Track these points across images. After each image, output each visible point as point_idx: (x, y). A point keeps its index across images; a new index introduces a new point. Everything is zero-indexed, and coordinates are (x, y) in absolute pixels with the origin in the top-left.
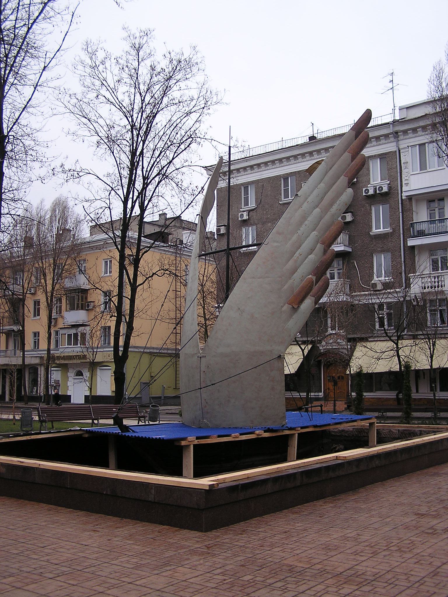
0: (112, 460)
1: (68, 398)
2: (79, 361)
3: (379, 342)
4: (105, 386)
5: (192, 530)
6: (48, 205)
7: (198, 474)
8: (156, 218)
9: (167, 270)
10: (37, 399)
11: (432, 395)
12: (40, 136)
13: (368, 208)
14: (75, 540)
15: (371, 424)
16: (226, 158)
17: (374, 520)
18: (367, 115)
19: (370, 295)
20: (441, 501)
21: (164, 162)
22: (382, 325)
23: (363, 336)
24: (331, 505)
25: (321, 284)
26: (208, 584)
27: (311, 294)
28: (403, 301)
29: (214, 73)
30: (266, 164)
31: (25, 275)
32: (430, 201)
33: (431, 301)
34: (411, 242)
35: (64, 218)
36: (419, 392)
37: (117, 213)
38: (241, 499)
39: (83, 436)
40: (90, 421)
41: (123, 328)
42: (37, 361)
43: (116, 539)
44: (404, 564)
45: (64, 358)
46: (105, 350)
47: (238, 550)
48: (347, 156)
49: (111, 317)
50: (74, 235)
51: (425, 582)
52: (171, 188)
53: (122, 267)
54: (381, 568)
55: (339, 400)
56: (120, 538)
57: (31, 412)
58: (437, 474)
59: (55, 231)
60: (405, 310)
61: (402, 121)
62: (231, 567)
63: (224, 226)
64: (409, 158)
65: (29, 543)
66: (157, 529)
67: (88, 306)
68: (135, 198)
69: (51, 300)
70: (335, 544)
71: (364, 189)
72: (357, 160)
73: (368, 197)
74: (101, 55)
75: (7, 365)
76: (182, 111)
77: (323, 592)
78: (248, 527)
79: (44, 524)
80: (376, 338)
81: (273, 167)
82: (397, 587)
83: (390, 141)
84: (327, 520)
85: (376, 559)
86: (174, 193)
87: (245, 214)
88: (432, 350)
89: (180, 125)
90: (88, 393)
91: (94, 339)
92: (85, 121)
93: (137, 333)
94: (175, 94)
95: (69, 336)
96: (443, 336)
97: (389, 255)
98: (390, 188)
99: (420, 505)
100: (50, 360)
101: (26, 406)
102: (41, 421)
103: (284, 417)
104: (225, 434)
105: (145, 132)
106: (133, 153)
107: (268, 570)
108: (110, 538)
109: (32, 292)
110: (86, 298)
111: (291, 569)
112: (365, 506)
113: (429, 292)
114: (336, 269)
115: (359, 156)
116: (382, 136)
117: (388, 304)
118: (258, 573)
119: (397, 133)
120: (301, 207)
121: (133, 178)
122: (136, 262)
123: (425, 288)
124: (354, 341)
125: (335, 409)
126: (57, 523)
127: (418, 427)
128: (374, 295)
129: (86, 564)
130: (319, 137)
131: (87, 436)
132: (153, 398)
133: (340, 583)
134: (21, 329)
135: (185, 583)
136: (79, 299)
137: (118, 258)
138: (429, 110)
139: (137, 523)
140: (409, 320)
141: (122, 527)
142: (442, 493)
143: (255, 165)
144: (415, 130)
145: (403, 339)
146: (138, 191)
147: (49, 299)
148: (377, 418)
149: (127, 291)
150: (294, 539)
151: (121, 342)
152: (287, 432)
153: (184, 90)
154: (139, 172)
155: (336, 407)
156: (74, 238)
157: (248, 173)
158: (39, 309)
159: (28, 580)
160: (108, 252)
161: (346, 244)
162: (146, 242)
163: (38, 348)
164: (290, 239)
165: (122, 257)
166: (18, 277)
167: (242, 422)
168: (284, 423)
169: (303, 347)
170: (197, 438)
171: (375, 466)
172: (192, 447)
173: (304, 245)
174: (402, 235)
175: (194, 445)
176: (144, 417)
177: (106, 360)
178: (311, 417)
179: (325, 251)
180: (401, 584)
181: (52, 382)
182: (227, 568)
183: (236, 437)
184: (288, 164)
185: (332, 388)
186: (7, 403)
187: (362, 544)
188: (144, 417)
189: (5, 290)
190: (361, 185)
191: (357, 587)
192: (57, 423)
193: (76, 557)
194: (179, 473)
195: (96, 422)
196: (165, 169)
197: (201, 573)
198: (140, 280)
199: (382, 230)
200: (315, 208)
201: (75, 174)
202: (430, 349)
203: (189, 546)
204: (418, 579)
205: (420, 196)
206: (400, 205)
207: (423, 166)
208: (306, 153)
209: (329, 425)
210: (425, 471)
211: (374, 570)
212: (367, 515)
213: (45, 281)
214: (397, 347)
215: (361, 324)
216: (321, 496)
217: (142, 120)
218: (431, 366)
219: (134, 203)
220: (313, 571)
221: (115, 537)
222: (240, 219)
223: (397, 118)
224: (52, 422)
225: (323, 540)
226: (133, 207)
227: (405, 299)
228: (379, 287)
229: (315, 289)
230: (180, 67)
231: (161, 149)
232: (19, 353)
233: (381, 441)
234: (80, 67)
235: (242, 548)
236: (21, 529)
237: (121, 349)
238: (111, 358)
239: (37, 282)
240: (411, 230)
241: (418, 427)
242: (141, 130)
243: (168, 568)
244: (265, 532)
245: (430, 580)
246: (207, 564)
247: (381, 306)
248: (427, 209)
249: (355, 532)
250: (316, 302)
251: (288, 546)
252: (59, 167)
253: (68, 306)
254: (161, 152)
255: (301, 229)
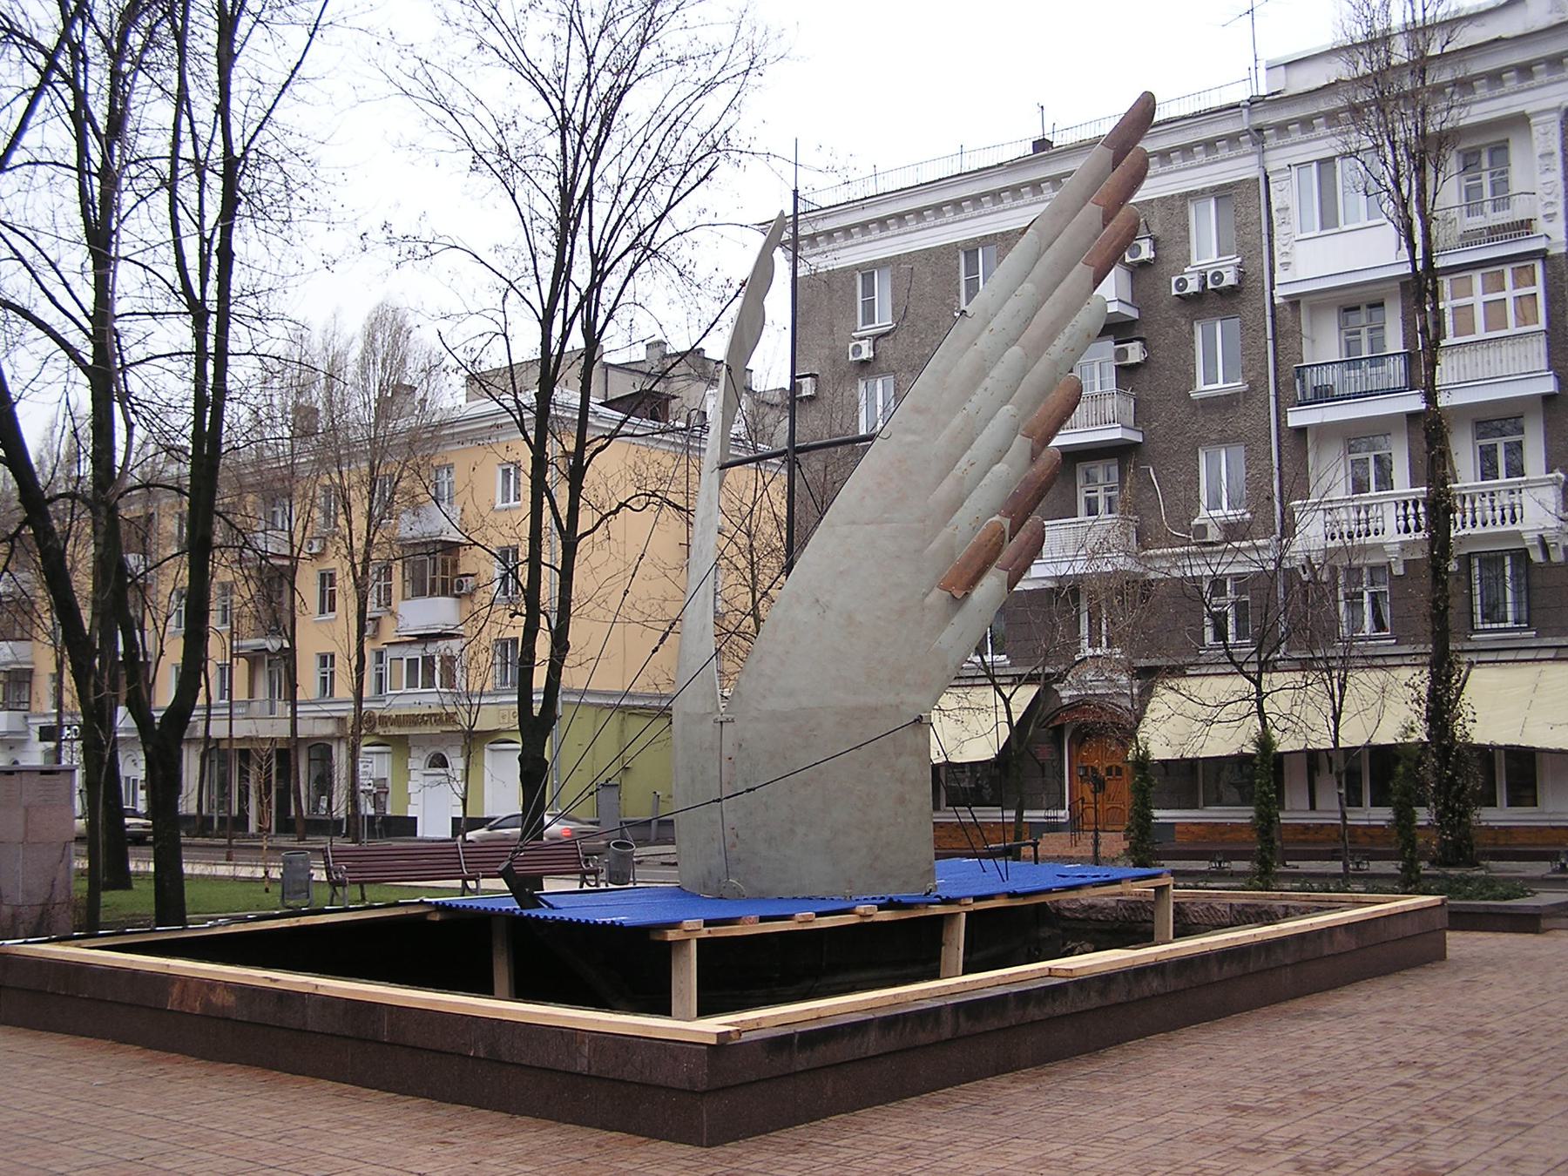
0: (502, 975)
1: (407, 825)
2: (437, 730)
3: (1212, 679)
4: (501, 792)
6: (352, 329)
7: (705, 1010)
8: (639, 353)
10: (329, 827)
12: (328, 158)
13: (1186, 328)
16: (789, 211)
19: (1188, 555)
20: (1301, 1076)
21: (646, 215)
22: (1221, 634)
24: (1029, 1087)
27: (998, 562)
28: (1275, 572)
31: (296, 508)
32: (1346, 310)
33: (1350, 570)
34: (1296, 418)
35: (396, 359)
36: (1318, 806)
37: (527, 345)
39: (429, 918)
40: (458, 883)
42: (328, 729)
43: (493, 1161)
45: (399, 721)
46: (499, 700)
49: (512, 616)
50: (424, 400)
52: (667, 281)
53: (540, 488)
57: (307, 860)
60: (1281, 595)
64: (1292, 197)
69: (365, 571)
71: (1174, 279)
76: (694, 79)
78: (815, 1136)
79: (323, 1126)
84: (1008, 1122)
86: (673, 294)
89: (686, 118)
92: (442, 115)
93: (577, 659)
95: (412, 663)
96: (1380, 662)
97: (1239, 451)
98: (1242, 276)
100: (362, 728)
101: (302, 845)
102: (334, 884)
103: (931, 872)
105: (596, 141)
106: (566, 195)
108: (477, 1159)
109: (315, 550)
110: (455, 566)
116: (1220, 138)
117: (1237, 578)
119: (1259, 130)
120: (973, 342)
122: (576, 476)
123: (1333, 538)
124: (1149, 677)
125: (1096, 852)
127: (1281, 898)
128: (1195, 555)
130: (1058, 141)
131: (437, 917)
134: (287, 645)
136: (437, 567)
137: (528, 466)
138: (1338, 70)
142: (1308, 1059)
144: (1306, 123)
145: (1275, 670)
147: (359, 568)
148: (1174, 873)
149: (552, 551)
150: (921, 1163)
151: (539, 679)
152: (939, 910)
154: (582, 239)
155: (1101, 849)
156: (423, 408)
158: (332, 593)
162: (604, 418)
163: (332, 694)
164: (945, 426)
165: (540, 463)
166: (279, 510)
168: (930, 886)
169: (1007, 691)
170: (707, 923)
171: (1147, 993)
172: (694, 944)
174: (1272, 400)
179: (1034, 456)
181: (365, 783)
183: (805, 920)
185: (1090, 797)
188: (596, 873)
189: (241, 548)
190: (1167, 267)
192: (375, 887)
194: (662, 1007)
195: (472, 884)
196: (649, 233)
198: (585, 520)
199: (1220, 384)
200: (1008, 346)
201: (420, 249)
202: (1332, 697)
206: (1269, 320)
207: (1329, 219)
208: (1024, 185)
209: (1049, 891)
210: (1284, 1006)
212: (1109, 1111)
213: (349, 522)
214: (1259, 692)
215: (1164, 629)
216: (1005, 1066)
217: (591, 103)
218: (1336, 742)
219: (568, 324)
221: (491, 1156)
224: (362, 884)
226: (565, 335)
227: (1279, 565)
228: (1213, 535)
229: (1009, 549)
236: (270, 1137)
237: (538, 697)
238: (514, 723)
239: (327, 525)
240: (1296, 384)
241: (1281, 898)
242: (584, 130)
244: (854, 1146)
247: (1218, 584)
249: (1071, 1149)
250: (1012, 583)
254: (638, 190)
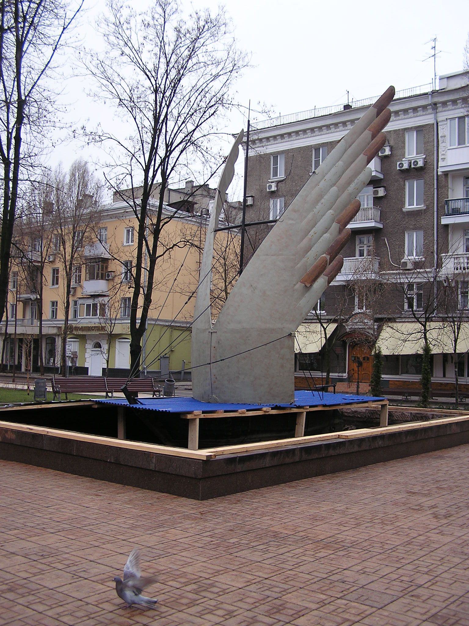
0: (121, 430)
1: (85, 370)
2: (97, 333)
4: (122, 359)
5: (189, 498)
6: (67, 169)
8: (182, 185)
9: (188, 242)
10: (54, 370)
11: (455, 380)
12: (60, 101)
13: (402, 183)
14: (77, 502)
15: (383, 406)
17: (366, 496)
18: (391, 91)
19: (399, 274)
20: (437, 481)
21: (191, 127)
22: (411, 306)
23: (390, 316)
24: (329, 481)
25: (335, 263)
26: (196, 544)
27: (324, 273)
29: (243, 32)
30: (297, 133)
31: (44, 242)
34: (445, 221)
36: (446, 376)
37: (139, 180)
38: (239, 471)
40: (104, 394)
41: (141, 301)
42: (54, 331)
43: (116, 503)
44: (382, 535)
45: (82, 329)
46: (123, 322)
47: (230, 517)
48: (367, 134)
51: (397, 549)
53: (142, 237)
54: (361, 537)
55: (363, 381)
56: (120, 502)
57: (44, 383)
58: (441, 457)
59: (75, 195)
61: (442, 92)
62: (220, 531)
63: (252, 196)
64: (447, 131)
65: (35, 503)
66: (156, 496)
67: (108, 276)
68: (157, 165)
69: (70, 269)
70: (323, 515)
71: (398, 163)
72: (378, 138)
73: (402, 171)
74: (125, 13)
75: (23, 334)
77: (300, 555)
78: (244, 498)
80: (403, 319)
81: (305, 136)
82: (370, 553)
83: (427, 113)
84: (320, 495)
85: (357, 530)
87: (273, 185)
88: (456, 334)
90: (105, 366)
91: (112, 310)
93: (154, 306)
94: (201, 56)
97: (421, 233)
98: (425, 163)
99: (414, 485)
100: (68, 331)
102: (55, 392)
103: (293, 396)
104: (232, 409)
106: (156, 118)
107: (254, 535)
108: (110, 502)
110: (107, 268)
111: (276, 535)
112: (361, 484)
113: (459, 274)
114: (365, 246)
115: (379, 134)
117: (418, 284)
118: (244, 537)
119: (435, 104)
120: (317, 185)
121: (155, 146)
122: (156, 233)
124: (381, 322)
125: (358, 391)
126: (62, 487)
127: (431, 411)
129: (86, 523)
131: (96, 407)
132: (173, 373)
133: (319, 548)
134: (39, 297)
135: (174, 543)
136: (100, 268)
139: (137, 490)
140: (438, 302)
141: (124, 493)
142: (440, 474)
143: (285, 134)
144: (454, 102)
145: (432, 321)
146: (161, 158)
147: (68, 267)
148: (389, 400)
149: (146, 263)
150: (285, 509)
152: (295, 410)
153: (214, 48)
154: (162, 137)
155: (360, 389)
157: (278, 142)
159: (32, 533)
160: (127, 222)
161: (377, 220)
163: (56, 318)
164: (305, 217)
167: (251, 398)
168: (292, 401)
170: (204, 412)
171: (377, 446)
172: (198, 421)
173: (319, 224)
174: (435, 213)
175: (200, 419)
176: (159, 391)
177: (124, 332)
178: (321, 397)
179: (340, 231)
180: (375, 550)
181: (68, 353)
182: (216, 531)
183: (242, 412)
184: (320, 133)
185: (356, 369)
186: (23, 373)
187: (349, 516)
188: (159, 391)
189: (22, 258)
191: (333, 552)
193: (77, 517)
194: (186, 446)
195: (110, 394)
197: (191, 534)
199: (415, 206)
200: (331, 186)
201: (96, 138)
202: (454, 332)
203: (185, 512)
204: (392, 547)
205: (456, 172)
206: (435, 181)
209: (339, 405)
210: (430, 453)
211: (353, 539)
212: (360, 492)
213: (65, 249)
214: (425, 329)
215: (389, 303)
219: (155, 172)
220: (296, 537)
221: (116, 501)
222: (268, 190)
223: (437, 89)
224: (66, 393)
225: (312, 511)
226: (154, 176)
227: (435, 279)
228: (409, 266)
229: (329, 268)
230: (208, 27)
231: (185, 115)
232: (36, 323)
233: (391, 423)
234: (104, 25)
235: (234, 516)
237: (138, 321)
238: (128, 331)
240: (445, 208)
241: (431, 411)
242: (164, 92)
243: (162, 529)
244: (259, 502)
245: (402, 548)
246: (198, 527)
247: (410, 286)
248: (464, 186)
249: (345, 506)
251: (279, 515)
252: (80, 128)
253: (88, 275)
255: (317, 207)
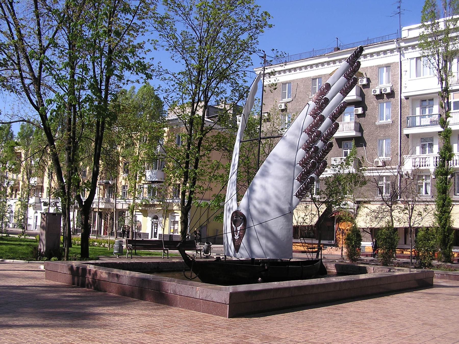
63: (267, 113)
71: (373, 90)
87: (283, 105)
117: (387, 177)
